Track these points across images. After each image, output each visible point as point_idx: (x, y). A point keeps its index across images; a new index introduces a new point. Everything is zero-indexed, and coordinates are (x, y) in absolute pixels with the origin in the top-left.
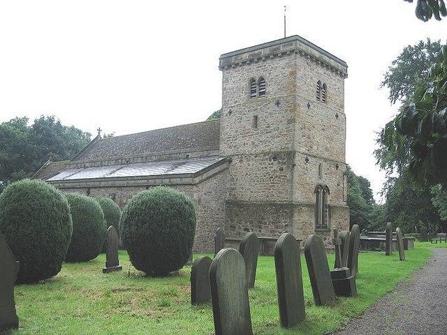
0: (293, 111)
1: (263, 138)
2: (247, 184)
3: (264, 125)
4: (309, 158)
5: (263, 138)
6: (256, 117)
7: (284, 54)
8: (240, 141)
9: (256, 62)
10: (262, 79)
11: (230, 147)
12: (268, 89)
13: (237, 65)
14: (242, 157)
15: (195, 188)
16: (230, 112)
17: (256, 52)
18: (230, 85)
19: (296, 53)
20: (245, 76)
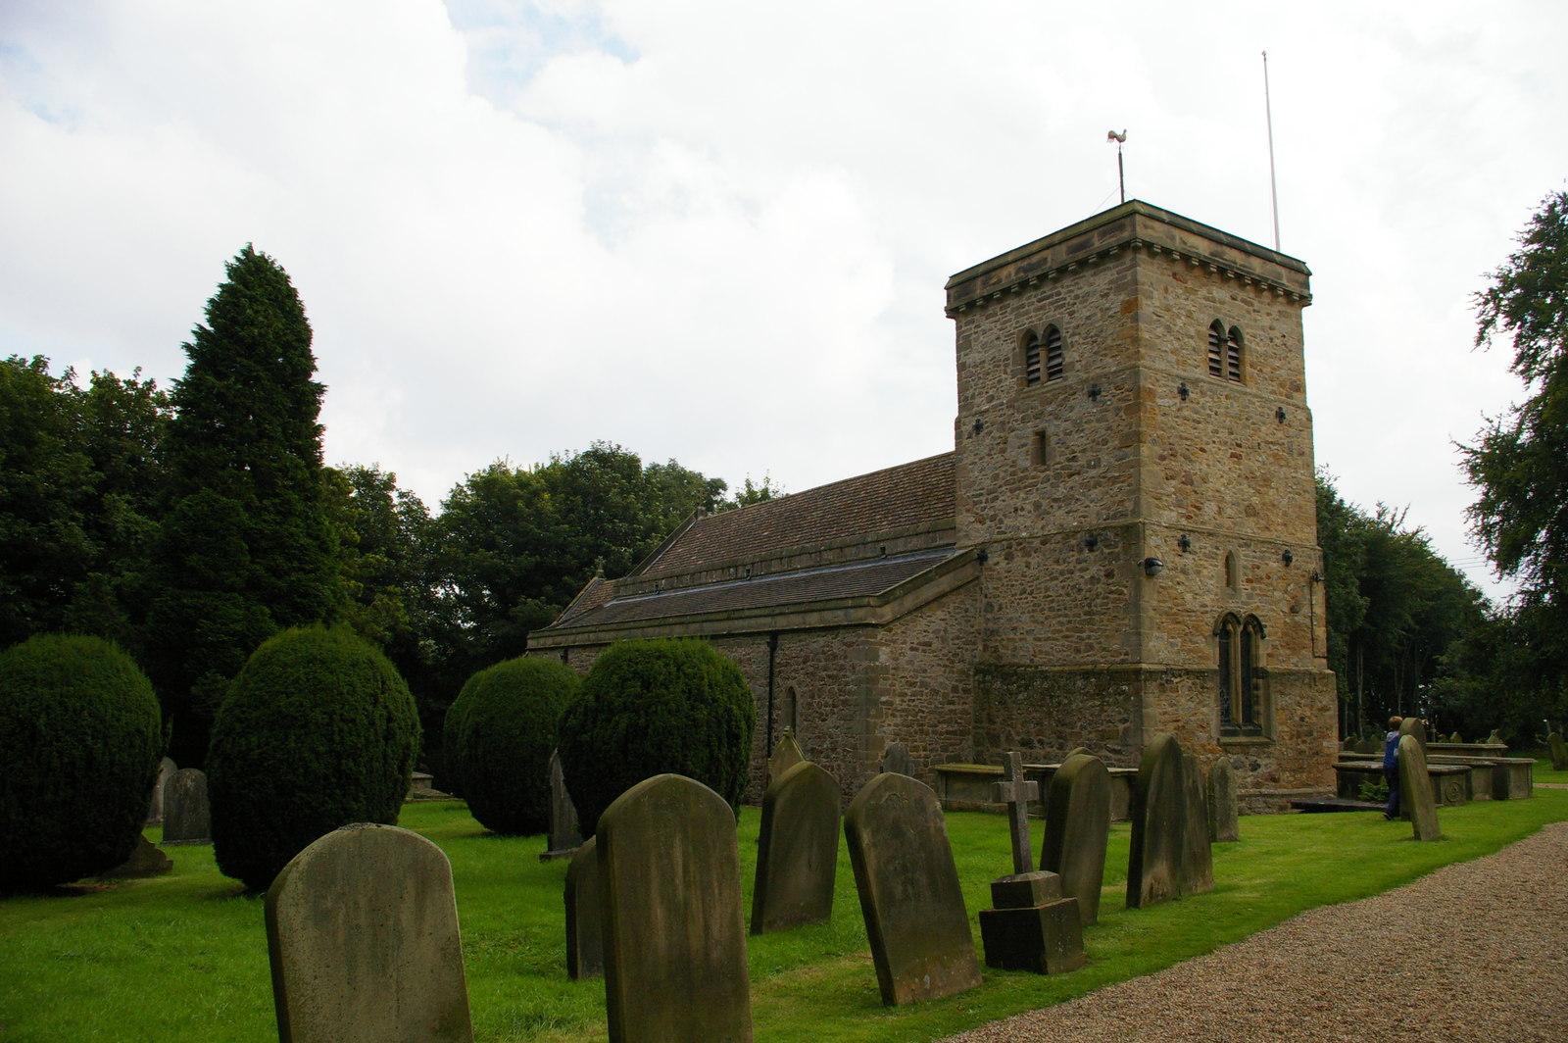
0: (1134, 409)
1: (1061, 491)
2: (1026, 617)
4: (1190, 538)
6: (1042, 436)
7: (1104, 256)
9: (1036, 287)
10: (1053, 331)
12: (1070, 356)
13: (988, 299)
14: (1013, 547)
15: (881, 634)
16: (978, 428)
17: (1035, 259)
18: (975, 357)
19: (1136, 249)
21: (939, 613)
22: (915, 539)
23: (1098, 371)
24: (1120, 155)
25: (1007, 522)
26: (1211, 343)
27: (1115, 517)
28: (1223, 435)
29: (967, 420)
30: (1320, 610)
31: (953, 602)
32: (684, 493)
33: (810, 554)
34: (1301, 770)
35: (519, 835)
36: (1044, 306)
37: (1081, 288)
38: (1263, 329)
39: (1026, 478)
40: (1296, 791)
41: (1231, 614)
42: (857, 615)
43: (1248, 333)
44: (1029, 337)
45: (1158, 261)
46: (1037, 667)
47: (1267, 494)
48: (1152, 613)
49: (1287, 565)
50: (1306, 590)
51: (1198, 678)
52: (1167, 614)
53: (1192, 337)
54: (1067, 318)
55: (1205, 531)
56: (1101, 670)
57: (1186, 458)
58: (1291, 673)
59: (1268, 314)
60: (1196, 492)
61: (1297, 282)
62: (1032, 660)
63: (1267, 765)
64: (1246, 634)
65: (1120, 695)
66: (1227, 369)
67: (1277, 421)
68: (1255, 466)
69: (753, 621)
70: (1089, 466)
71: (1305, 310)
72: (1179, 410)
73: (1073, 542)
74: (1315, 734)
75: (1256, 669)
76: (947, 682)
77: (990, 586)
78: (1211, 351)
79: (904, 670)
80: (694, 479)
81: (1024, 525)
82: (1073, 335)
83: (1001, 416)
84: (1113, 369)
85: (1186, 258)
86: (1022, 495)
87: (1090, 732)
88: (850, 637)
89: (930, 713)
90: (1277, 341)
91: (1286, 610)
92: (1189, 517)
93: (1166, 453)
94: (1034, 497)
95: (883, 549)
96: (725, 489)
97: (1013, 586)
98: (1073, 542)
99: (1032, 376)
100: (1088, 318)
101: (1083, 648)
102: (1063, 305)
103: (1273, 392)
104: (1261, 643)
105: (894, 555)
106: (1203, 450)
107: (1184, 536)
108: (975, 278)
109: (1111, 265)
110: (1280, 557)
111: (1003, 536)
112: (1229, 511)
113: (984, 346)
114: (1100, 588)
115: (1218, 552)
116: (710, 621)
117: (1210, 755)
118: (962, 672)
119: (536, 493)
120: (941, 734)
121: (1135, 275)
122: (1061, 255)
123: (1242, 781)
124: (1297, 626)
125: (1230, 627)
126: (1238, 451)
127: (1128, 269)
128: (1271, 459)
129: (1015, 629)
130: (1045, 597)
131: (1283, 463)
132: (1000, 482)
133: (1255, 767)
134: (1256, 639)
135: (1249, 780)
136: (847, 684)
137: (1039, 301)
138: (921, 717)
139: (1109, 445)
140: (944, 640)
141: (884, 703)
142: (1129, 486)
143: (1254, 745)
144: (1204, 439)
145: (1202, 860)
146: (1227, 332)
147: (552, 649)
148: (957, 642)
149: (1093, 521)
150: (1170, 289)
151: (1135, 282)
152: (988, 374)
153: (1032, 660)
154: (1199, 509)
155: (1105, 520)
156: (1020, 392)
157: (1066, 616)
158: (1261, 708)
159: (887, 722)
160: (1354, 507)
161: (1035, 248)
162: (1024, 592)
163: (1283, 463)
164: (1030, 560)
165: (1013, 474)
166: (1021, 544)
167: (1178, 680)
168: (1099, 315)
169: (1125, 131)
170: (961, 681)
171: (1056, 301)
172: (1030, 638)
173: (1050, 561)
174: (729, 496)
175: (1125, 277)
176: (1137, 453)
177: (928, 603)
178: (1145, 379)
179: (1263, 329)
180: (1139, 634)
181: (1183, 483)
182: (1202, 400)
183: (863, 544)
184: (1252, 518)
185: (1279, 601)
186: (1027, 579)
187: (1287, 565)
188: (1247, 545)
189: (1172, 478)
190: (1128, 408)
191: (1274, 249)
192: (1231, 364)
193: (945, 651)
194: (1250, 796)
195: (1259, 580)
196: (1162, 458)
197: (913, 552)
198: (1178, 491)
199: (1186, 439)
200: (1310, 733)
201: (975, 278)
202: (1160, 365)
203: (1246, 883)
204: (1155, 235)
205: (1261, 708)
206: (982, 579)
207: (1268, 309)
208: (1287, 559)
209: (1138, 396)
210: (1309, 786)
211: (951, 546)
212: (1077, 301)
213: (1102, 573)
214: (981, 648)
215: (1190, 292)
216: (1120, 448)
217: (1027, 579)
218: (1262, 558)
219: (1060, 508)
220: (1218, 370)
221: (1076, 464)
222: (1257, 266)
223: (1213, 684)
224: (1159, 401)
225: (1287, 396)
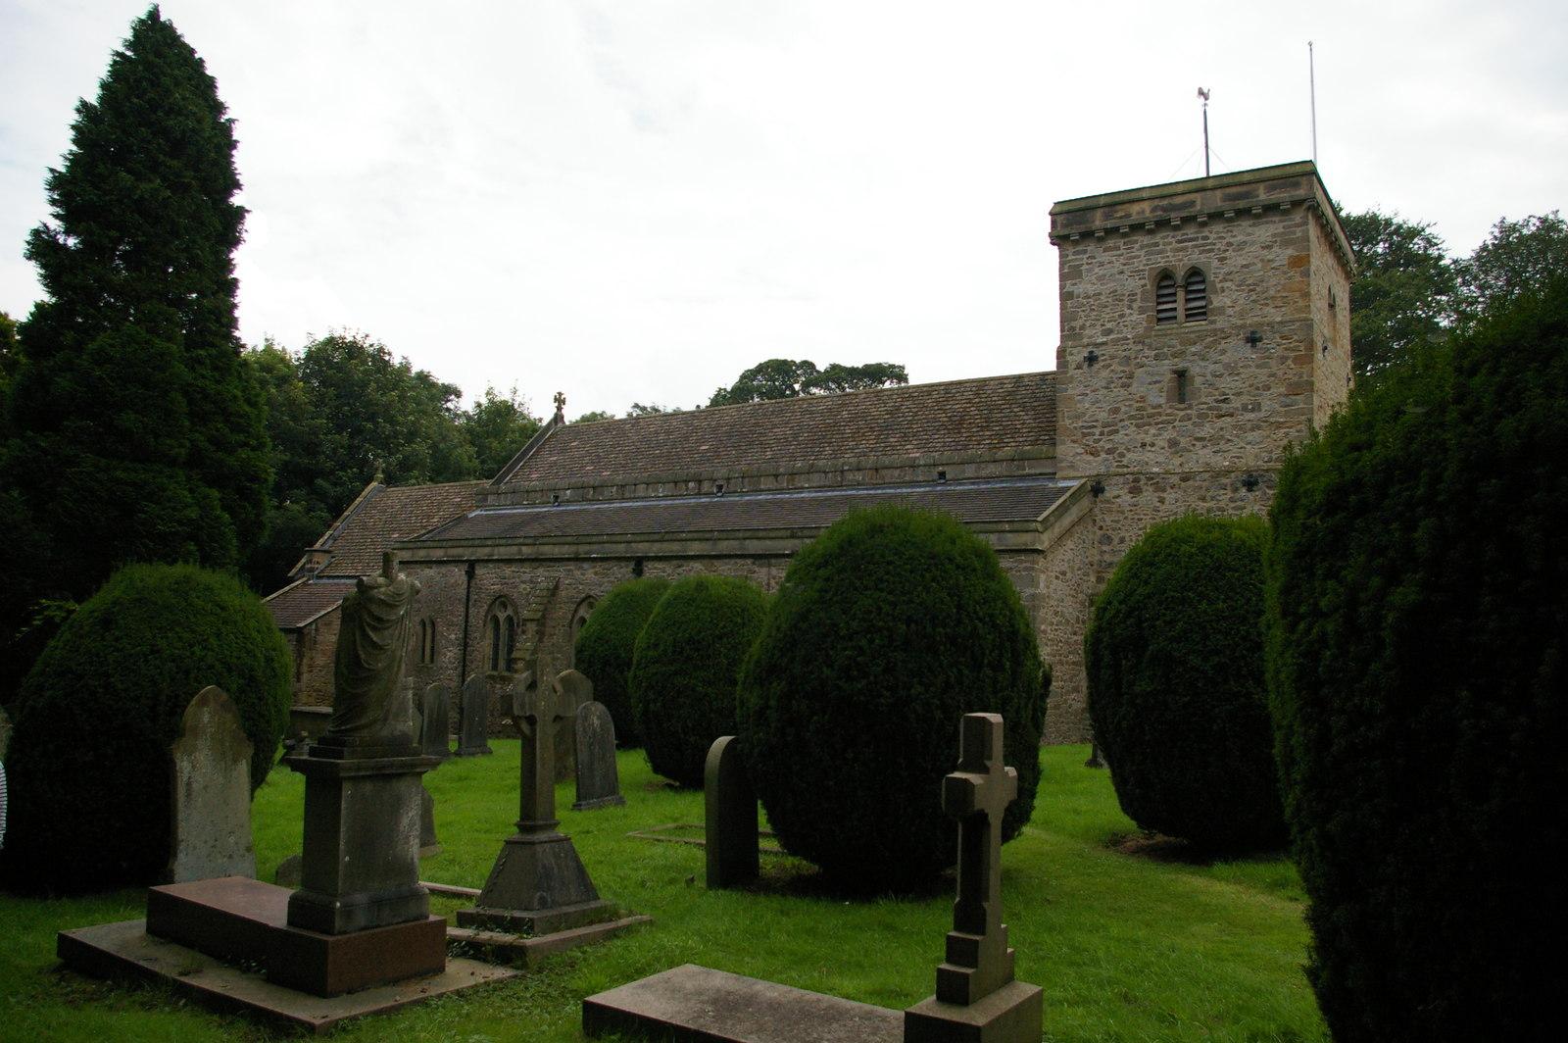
1: (1207, 430)
3: (1209, 394)
5: (1207, 430)
6: (1181, 375)
7: (1271, 209)
11: (1094, 453)
16: (1091, 359)
17: (1178, 200)
22: (992, 466)
23: (1255, 319)
24: (1205, 112)
25: (1129, 455)
29: (1075, 351)
36: (1187, 247)
37: (1235, 236)
39: (1160, 414)
54: (1216, 263)
73: (1225, 481)
81: (1155, 461)
82: (1225, 280)
94: (1167, 435)
95: (942, 475)
98: (1225, 481)
102: (1211, 251)
105: (957, 481)
109: (1276, 219)
113: (1100, 278)
122: (1216, 201)
132: (1120, 416)
142: (1298, 432)
152: (1106, 307)
161: (1180, 189)
164: (1165, 495)
166: (1152, 479)
171: (1203, 245)
186: (1161, 514)
197: (988, 479)
212: (1231, 249)
216: (1287, 395)
221: (1228, 406)
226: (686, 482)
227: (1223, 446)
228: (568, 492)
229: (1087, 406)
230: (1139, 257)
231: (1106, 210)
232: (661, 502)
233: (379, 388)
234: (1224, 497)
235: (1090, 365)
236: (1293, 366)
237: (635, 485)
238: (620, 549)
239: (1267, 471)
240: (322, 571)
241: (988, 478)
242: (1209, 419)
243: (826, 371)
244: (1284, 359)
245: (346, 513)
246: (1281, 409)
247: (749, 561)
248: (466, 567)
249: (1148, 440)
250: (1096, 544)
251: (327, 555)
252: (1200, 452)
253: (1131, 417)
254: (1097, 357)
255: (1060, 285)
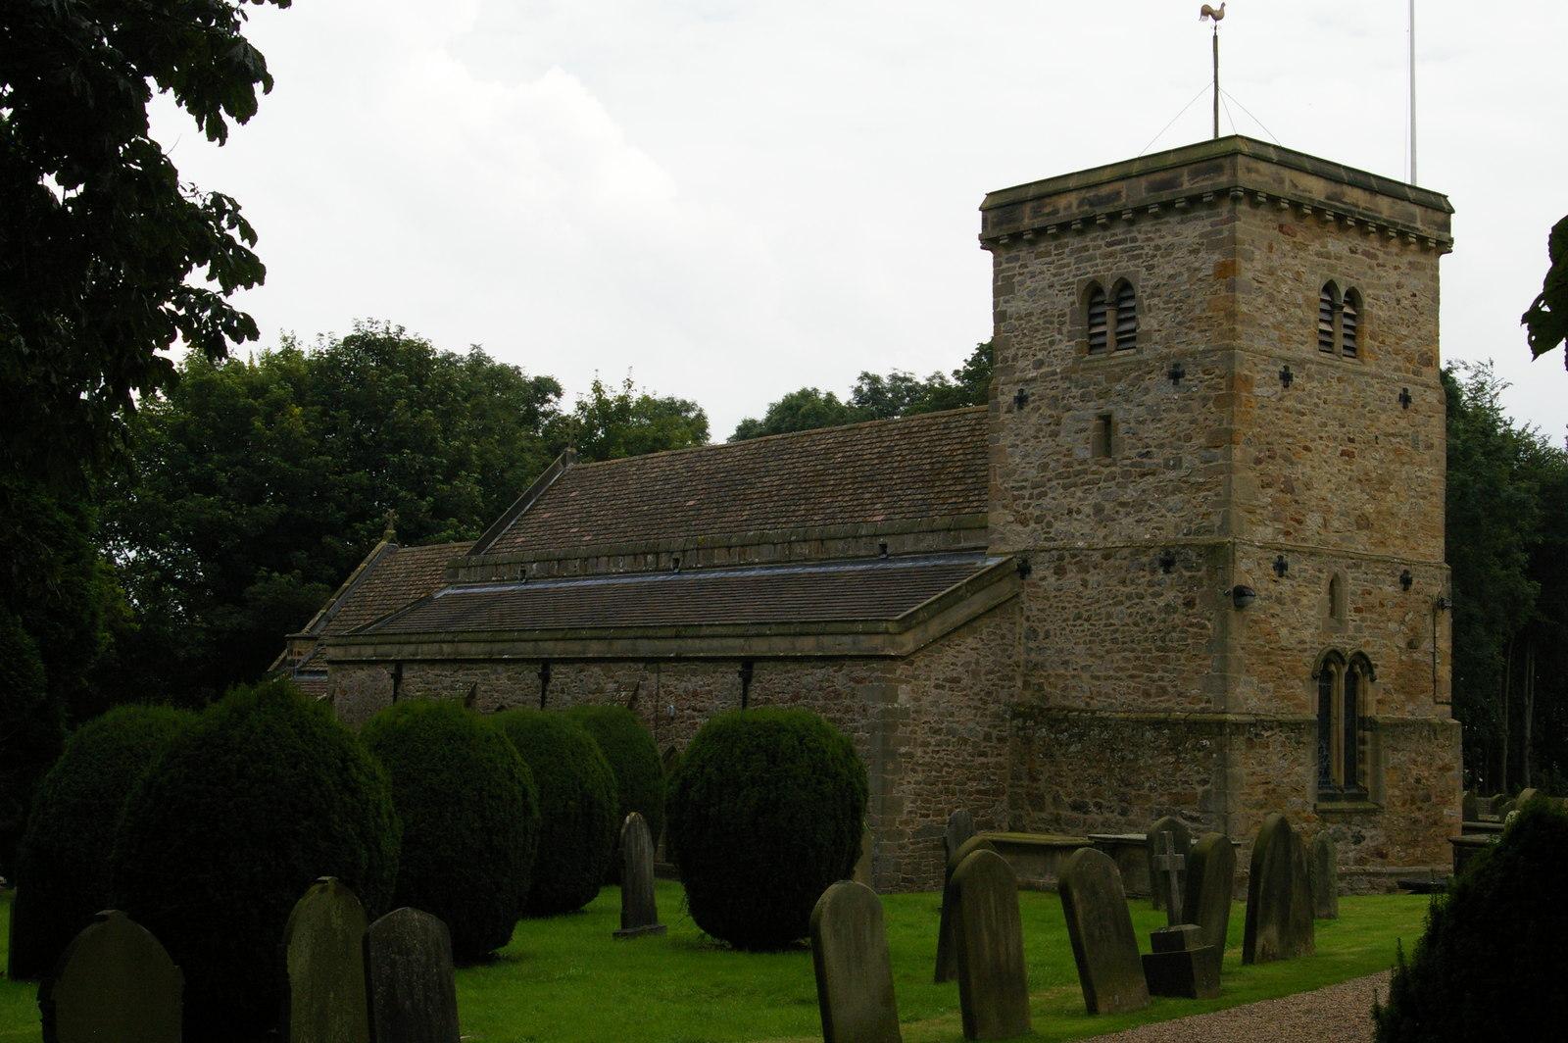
1: (1130, 494)
2: (1080, 649)
3: (1133, 447)
4: (1288, 559)
5: (1130, 494)
6: (1107, 420)
8: (1056, 498)
9: (1105, 227)
10: (1124, 286)
11: (1024, 523)
12: (1146, 323)
13: (1040, 233)
15: (901, 669)
16: (1021, 400)
17: (1105, 190)
19: (1236, 199)
20: (1069, 275)
21: (970, 640)
22: (930, 537)
23: (1182, 347)
24: (1215, 38)
25: (1057, 525)
26: (1322, 310)
27: (1197, 532)
28: (1333, 428)
29: (1006, 389)
30: (1445, 645)
31: (985, 629)
32: (500, 397)
33: (775, 544)
34: (1414, 843)
35: (539, 918)
38: (1388, 288)
39: (1085, 472)
40: (1407, 869)
41: (1335, 652)
42: (868, 644)
43: (1369, 296)
44: (1094, 290)
45: (1262, 212)
46: (1093, 712)
47: (1383, 499)
48: (1240, 653)
49: (1406, 589)
50: (1429, 619)
51: (1292, 731)
52: (1259, 653)
53: (1299, 306)
55: (1306, 550)
56: (1177, 720)
57: (1286, 459)
58: (1405, 724)
59: (1396, 268)
60: (1296, 502)
61: (1435, 223)
62: (1088, 704)
63: (1374, 837)
64: (1352, 679)
65: (1199, 751)
66: (1340, 342)
67: (1400, 406)
68: (1370, 464)
69: (715, 643)
70: (1167, 466)
71: (1444, 259)
72: (1280, 399)
73: (1144, 559)
74: (1434, 799)
75: (1363, 720)
76: (979, 729)
77: (1033, 607)
78: (1321, 320)
79: (927, 713)
80: (505, 377)
81: (1080, 532)
82: (1152, 296)
83: (1053, 389)
84: (1201, 347)
85: (1296, 206)
86: (1079, 494)
87: (1162, 795)
88: (860, 671)
89: (958, 766)
90: (1405, 302)
91: (1403, 645)
92: (1287, 534)
93: (1263, 454)
94: (1094, 498)
95: (884, 547)
96: (558, 394)
97: (1064, 608)
98: (1144, 559)
99: (1095, 341)
100: (1171, 277)
101: (1153, 691)
102: (1139, 256)
103: (1397, 369)
104: (1370, 687)
105: (899, 556)
106: (1307, 449)
107: (1281, 558)
108: (1023, 202)
109: (1204, 213)
110: (1398, 579)
111: (1052, 544)
112: (1336, 524)
113: (1032, 293)
114: (1177, 618)
115: (1321, 575)
116: (648, 638)
117: (1304, 825)
118: (996, 715)
119: (279, 406)
120: (970, 794)
121: (1233, 231)
122: (1138, 192)
123: (1344, 855)
124: (1415, 663)
125: (1333, 668)
126: (1350, 447)
127: (1226, 222)
128: (1391, 456)
129: (1065, 663)
130: (1106, 625)
131: (1405, 459)
132: (1049, 474)
133: (1358, 839)
134: (1365, 683)
135: (1350, 854)
136: (856, 730)
137: (1109, 245)
138: (947, 772)
139: (1193, 441)
140: (975, 674)
141: (903, 755)
142: (1216, 495)
143: (1357, 812)
144: (1310, 434)
145: (1304, 931)
146: (1343, 294)
147: (370, 663)
148: (990, 677)
149: (1168, 535)
150: (1275, 246)
151: (1233, 240)
152: (1037, 331)
153: (1088, 704)
154: (1300, 522)
155: (1185, 535)
156: (1077, 361)
157: (1133, 650)
158: (1368, 768)
159: (907, 779)
160: (1529, 431)
162: (1078, 617)
163: (1405, 459)
165: (1068, 465)
167: (1269, 733)
168: (1186, 276)
169: (1223, 5)
170: (995, 727)
171: (1132, 249)
172: (1085, 676)
173: (1114, 582)
174: (566, 406)
175: (1220, 232)
176: (1228, 456)
177: (956, 630)
178: (1241, 364)
179: (1388, 288)
180: (1224, 678)
181: (1282, 491)
182: (1308, 386)
183: (855, 537)
184: (1364, 532)
185: (1393, 635)
186: (1084, 601)
187: (1406, 589)
188: (1357, 566)
189: (1269, 485)
190: (1218, 399)
191: (1409, 182)
192: (1346, 336)
193: (976, 689)
194: (1352, 874)
195: (1371, 608)
196: (1258, 461)
197: (927, 554)
198: (1275, 500)
199: (1288, 436)
200: (1427, 798)
201: (1023, 202)
202: (1260, 344)
203: (1345, 951)
204: (1259, 179)
205: (1368, 768)
206: (1023, 596)
207: (1396, 260)
208: (1406, 581)
209: (1231, 387)
210: (1424, 863)
211: (980, 551)
213: (1180, 601)
214: (1020, 684)
215: (1304, 247)
217: (1084, 601)
218: (1374, 582)
219: (1128, 514)
220: (1330, 345)
222: (1385, 207)
223: (1310, 738)
224: (1257, 391)
225: (1416, 373)
226: (645, 554)
227: (1146, 514)
228: (534, 565)
229: (1018, 460)
230: (1068, 265)
231: (1035, 204)
232: (619, 579)
233: (410, 406)
234: (1142, 580)
235: (1021, 408)
236: (1213, 410)
237: (597, 557)
238: (527, 649)
239: (1184, 546)
240: (305, 665)
241: (926, 552)
242: (1132, 479)
243: (768, 420)
244: (1205, 399)
245: (345, 585)
246: (1202, 466)
247: (641, 666)
248: (392, 669)
249: (1074, 506)
250: (1023, 640)
251: (311, 643)
252: (1123, 522)
253: (1059, 476)
254: (1026, 397)
255: (994, 302)
